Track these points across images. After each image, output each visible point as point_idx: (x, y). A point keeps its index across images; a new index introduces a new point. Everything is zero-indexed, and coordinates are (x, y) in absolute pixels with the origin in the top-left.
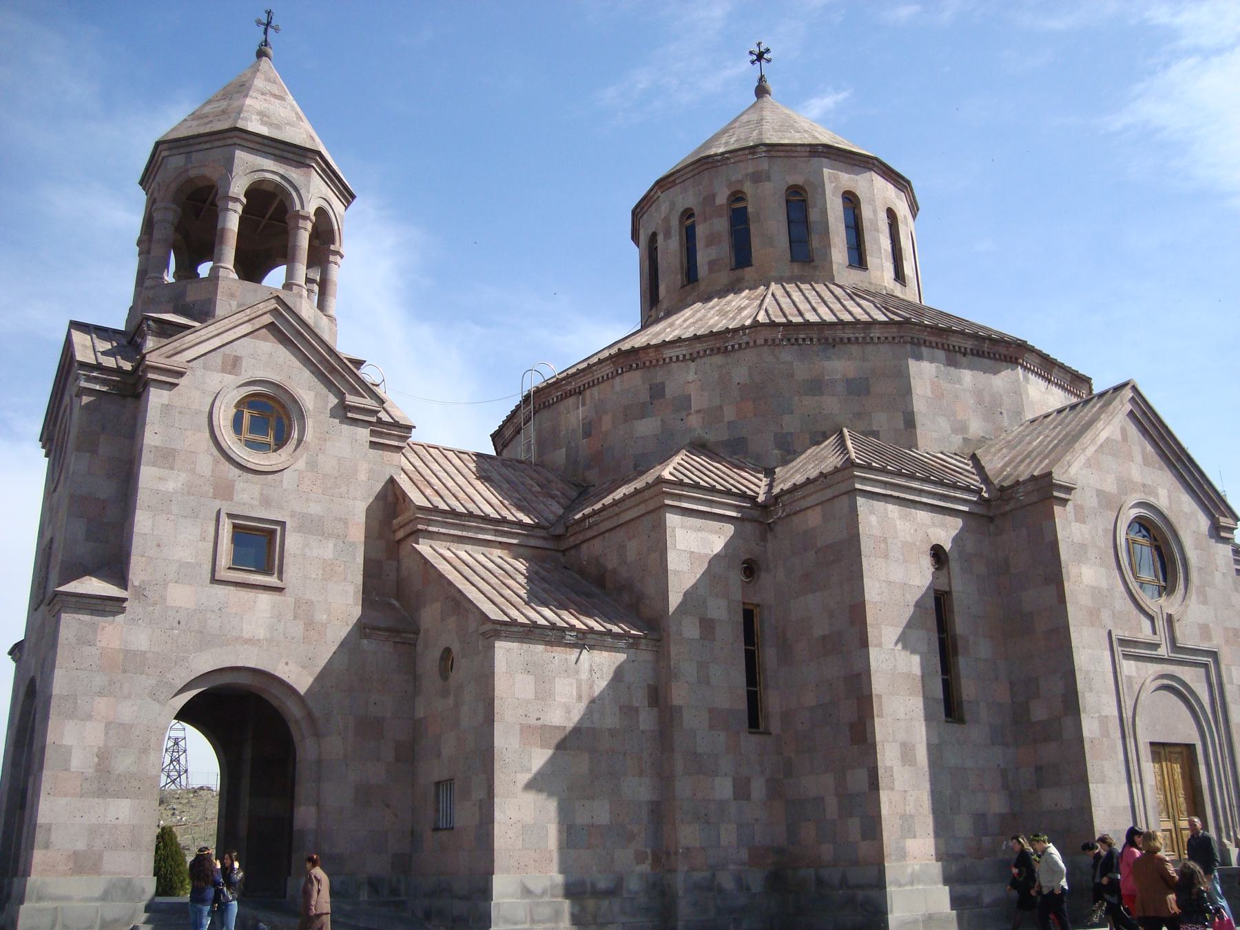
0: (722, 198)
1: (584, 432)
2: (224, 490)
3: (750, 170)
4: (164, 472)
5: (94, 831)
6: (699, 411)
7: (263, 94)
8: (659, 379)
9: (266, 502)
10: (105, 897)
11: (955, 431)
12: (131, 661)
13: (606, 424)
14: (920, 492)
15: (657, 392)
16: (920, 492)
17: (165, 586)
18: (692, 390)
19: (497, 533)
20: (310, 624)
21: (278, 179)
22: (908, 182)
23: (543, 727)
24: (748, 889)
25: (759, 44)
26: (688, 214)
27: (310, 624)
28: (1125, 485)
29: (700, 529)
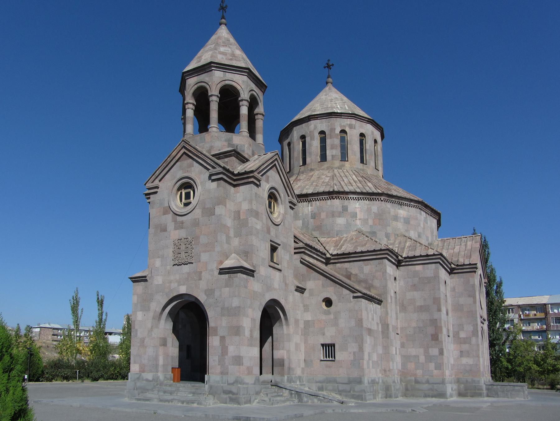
0: (338, 131)
1: (312, 216)
2: (269, 232)
3: (349, 123)
6: (360, 219)
13: (323, 215)
15: (345, 209)
20: (286, 284)
21: (196, 86)
27: (286, 284)
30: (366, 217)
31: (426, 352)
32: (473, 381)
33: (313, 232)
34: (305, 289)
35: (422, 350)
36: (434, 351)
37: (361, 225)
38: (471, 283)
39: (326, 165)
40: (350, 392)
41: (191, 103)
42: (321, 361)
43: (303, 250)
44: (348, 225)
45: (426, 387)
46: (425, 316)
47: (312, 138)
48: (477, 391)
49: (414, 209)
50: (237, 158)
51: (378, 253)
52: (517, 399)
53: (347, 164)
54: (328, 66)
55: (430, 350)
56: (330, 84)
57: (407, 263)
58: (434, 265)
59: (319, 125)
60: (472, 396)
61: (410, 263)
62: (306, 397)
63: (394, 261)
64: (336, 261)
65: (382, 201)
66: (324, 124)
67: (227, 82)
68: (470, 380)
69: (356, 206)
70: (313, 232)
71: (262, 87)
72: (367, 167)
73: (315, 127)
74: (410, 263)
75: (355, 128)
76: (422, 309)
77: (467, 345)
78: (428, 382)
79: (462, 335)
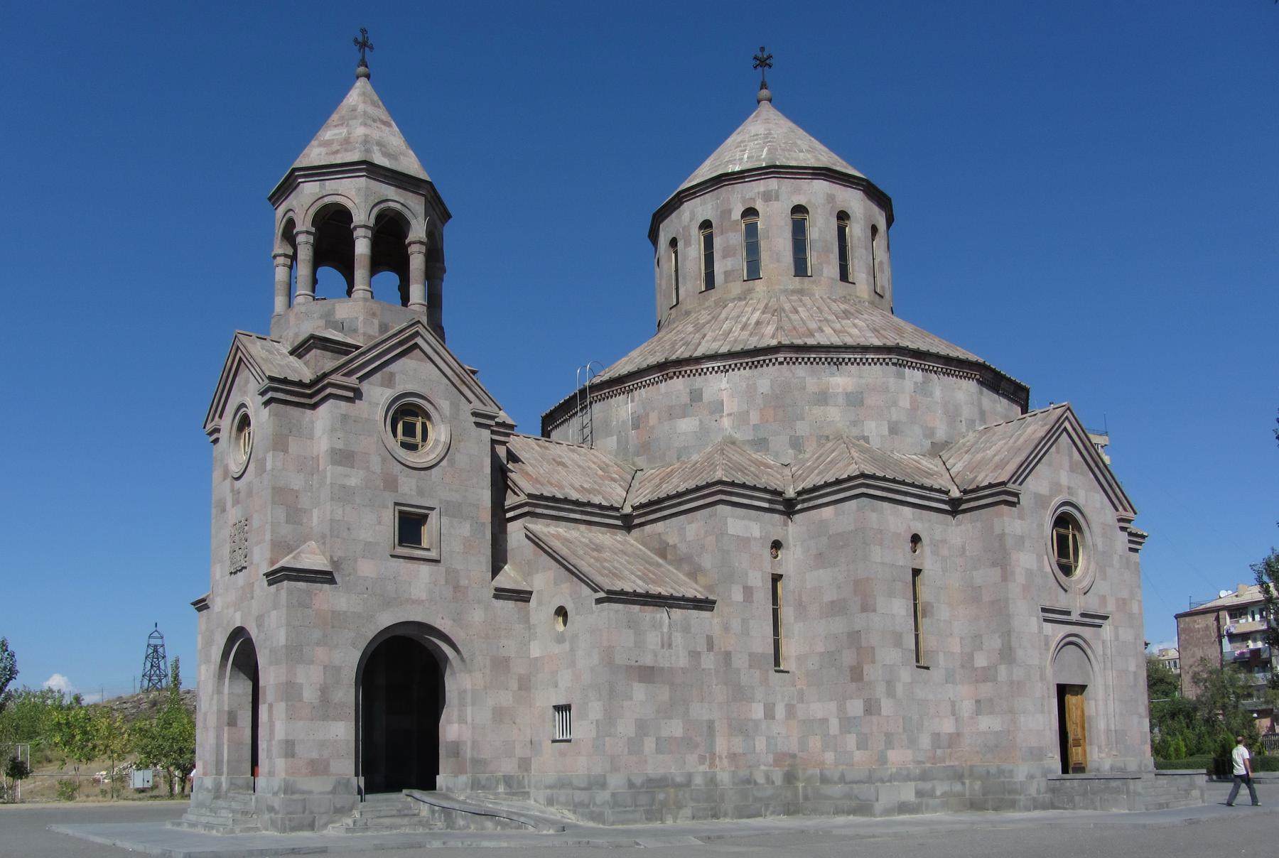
0: (736, 215)
2: (391, 483)
3: (762, 189)
4: (347, 470)
5: (322, 744)
6: (730, 415)
7: (374, 121)
8: (697, 386)
9: (421, 492)
10: (333, 792)
11: (925, 436)
12: (337, 620)
14: (906, 494)
15: (696, 396)
16: (906, 494)
17: (356, 561)
18: (725, 396)
19: (583, 513)
20: (457, 588)
22: (889, 200)
23: (640, 667)
24: (773, 783)
25: (762, 49)
26: (706, 225)
27: (457, 588)
28: (1056, 487)
29: (743, 518)
30: (745, 407)
31: (842, 709)
32: (1001, 772)
33: (636, 459)
34: (531, 593)
35: (833, 706)
36: (856, 707)
37: (733, 428)
38: (997, 531)
39: (714, 295)
40: (588, 806)
41: (280, 255)
42: (554, 741)
43: (526, 509)
44: (704, 431)
45: (837, 790)
46: (838, 625)
47: (688, 243)
48: (1007, 797)
49: (877, 368)
50: (325, 349)
51: (706, 492)
52: (1115, 810)
53: (759, 286)
54: (763, 63)
55: (848, 703)
56: (763, 103)
57: (806, 505)
58: (854, 502)
59: (700, 209)
60: (996, 809)
61: (811, 504)
62: (464, 818)
63: (766, 505)
64: (643, 520)
65: (781, 363)
66: (709, 206)
67: (327, 200)
68: (993, 770)
69: (722, 386)
70: (636, 459)
71: (419, 187)
72: (813, 282)
73: (693, 214)
74: (811, 504)
75: (777, 199)
76: (836, 608)
77: (990, 684)
78: (842, 779)
79: (981, 661)
